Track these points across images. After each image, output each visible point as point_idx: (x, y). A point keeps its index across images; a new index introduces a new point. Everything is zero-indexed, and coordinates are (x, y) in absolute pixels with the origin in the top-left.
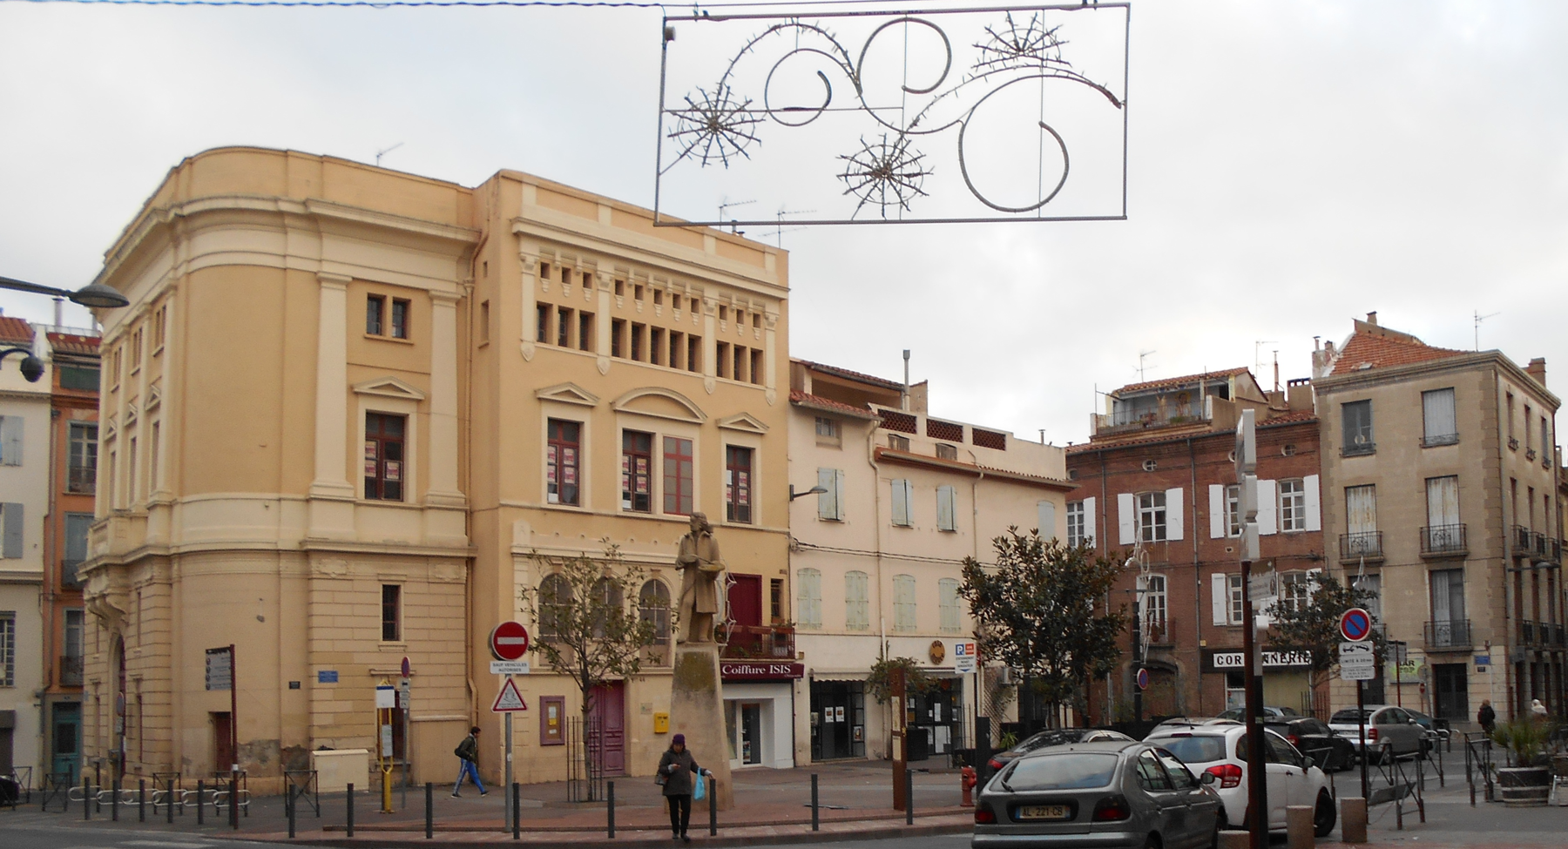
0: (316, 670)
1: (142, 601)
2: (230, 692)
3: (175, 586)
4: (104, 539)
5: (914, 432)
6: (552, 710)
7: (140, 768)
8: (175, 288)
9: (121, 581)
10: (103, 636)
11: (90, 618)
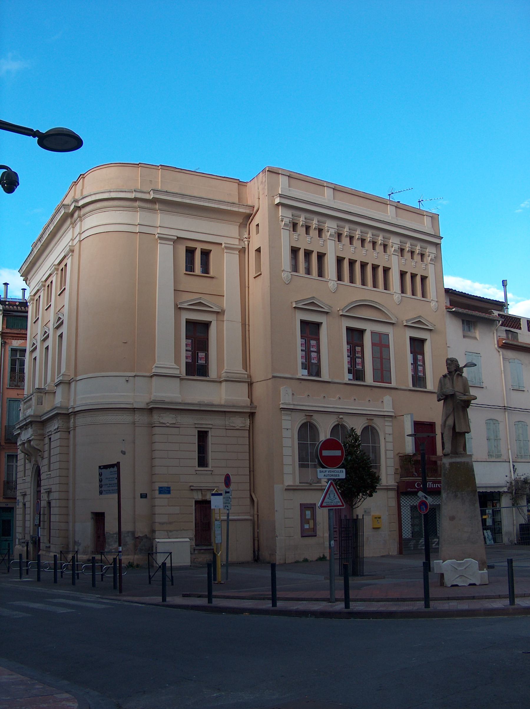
0: (157, 486)
1: (52, 443)
2: (117, 495)
3: (72, 432)
4: (30, 407)
5: (520, 328)
6: (308, 513)
7: (50, 547)
8: (72, 251)
9: (40, 432)
10: (28, 466)
11: (21, 456)
